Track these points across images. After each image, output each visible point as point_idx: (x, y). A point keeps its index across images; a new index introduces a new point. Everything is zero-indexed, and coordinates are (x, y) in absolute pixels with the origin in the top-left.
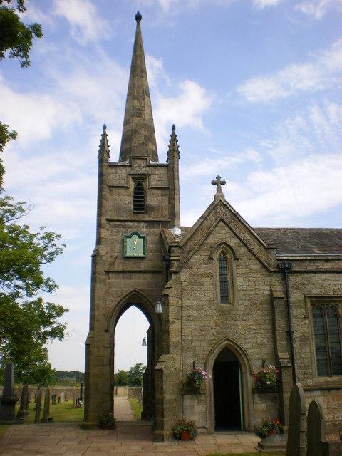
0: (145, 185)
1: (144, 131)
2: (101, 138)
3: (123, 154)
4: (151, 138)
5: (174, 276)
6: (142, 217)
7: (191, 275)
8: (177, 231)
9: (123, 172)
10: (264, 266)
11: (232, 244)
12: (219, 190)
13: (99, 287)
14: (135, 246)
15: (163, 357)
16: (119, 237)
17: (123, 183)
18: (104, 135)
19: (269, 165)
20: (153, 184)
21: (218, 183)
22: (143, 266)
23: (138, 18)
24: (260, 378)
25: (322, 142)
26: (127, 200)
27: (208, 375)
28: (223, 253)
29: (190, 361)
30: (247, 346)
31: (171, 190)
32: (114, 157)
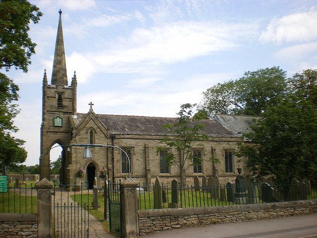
0: (62, 96)
1: (62, 72)
2: (44, 75)
3: (53, 81)
4: (65, 75)
5: (74, 138)
6: (61, 110)
7: (80, 138)
8: (75, 117)
9: (53, 91)
10: (105, 136)
11: (95, 128)
12: (91, 106)
13: (44, 138)
14: (58, 122)
15: (70, 165)
16: (51, 118)
17: (53, 95)
18: (45, 74)
19: (149, 24)
20: (66, 96)
21: (91, 104)
22: (61, 130)
23: (60, 12)
24: (102, 173)
25: (190, 12)
26: (55, 102)
27: (85, 172)
28: (91, 130)
29: (78, 166)
30: (98, 162)
31: (73, 100)
32: (49, 83)
